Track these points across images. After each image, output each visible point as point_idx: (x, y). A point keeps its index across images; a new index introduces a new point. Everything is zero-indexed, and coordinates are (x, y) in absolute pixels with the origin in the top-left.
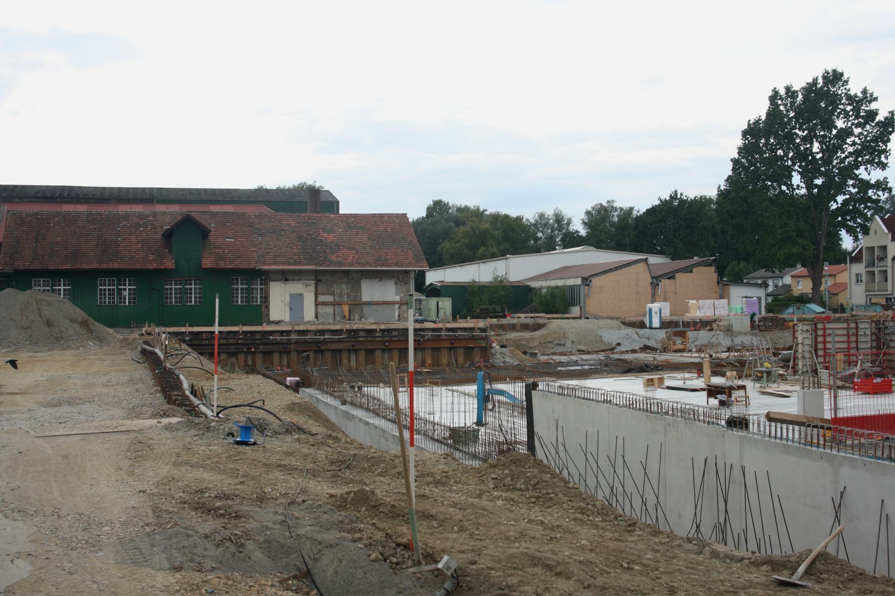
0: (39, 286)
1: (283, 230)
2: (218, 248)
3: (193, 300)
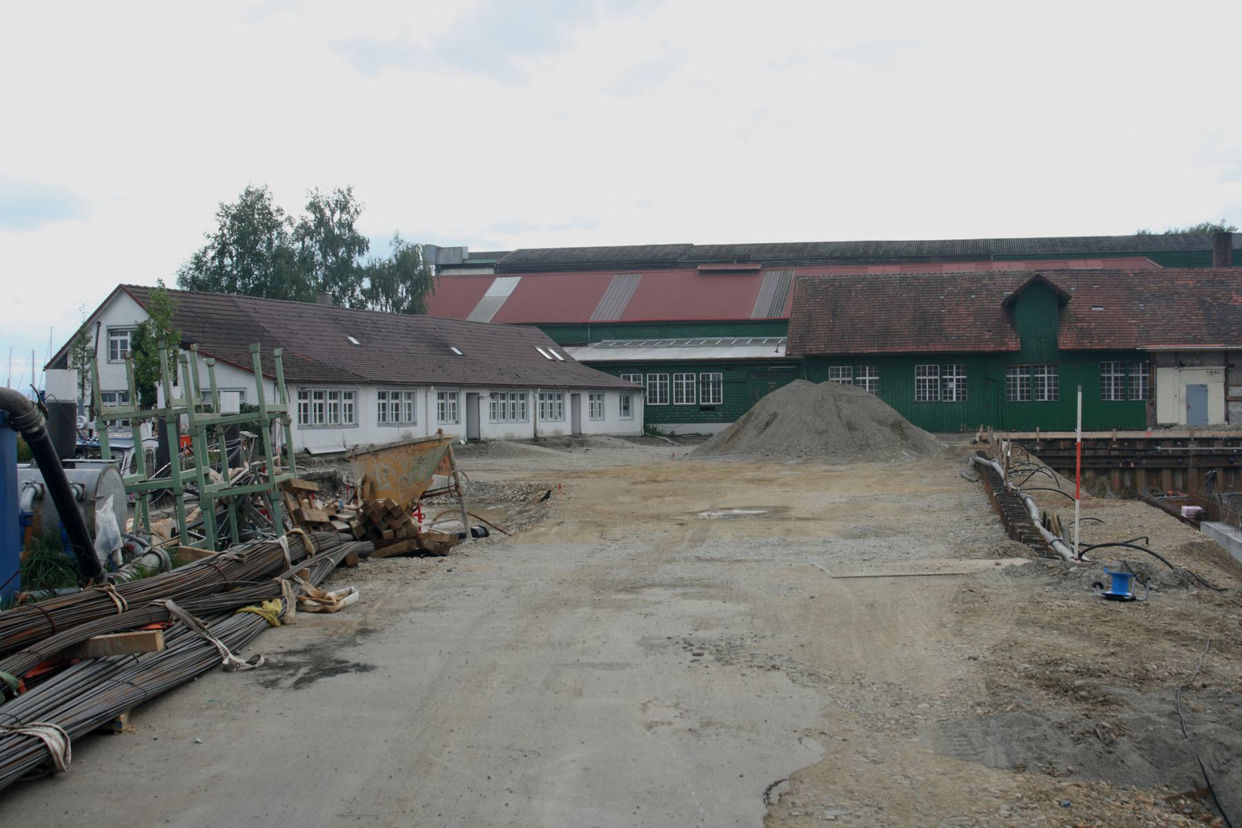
0: (838, 376)
1: (1176, 293)
3: (1046, 394)
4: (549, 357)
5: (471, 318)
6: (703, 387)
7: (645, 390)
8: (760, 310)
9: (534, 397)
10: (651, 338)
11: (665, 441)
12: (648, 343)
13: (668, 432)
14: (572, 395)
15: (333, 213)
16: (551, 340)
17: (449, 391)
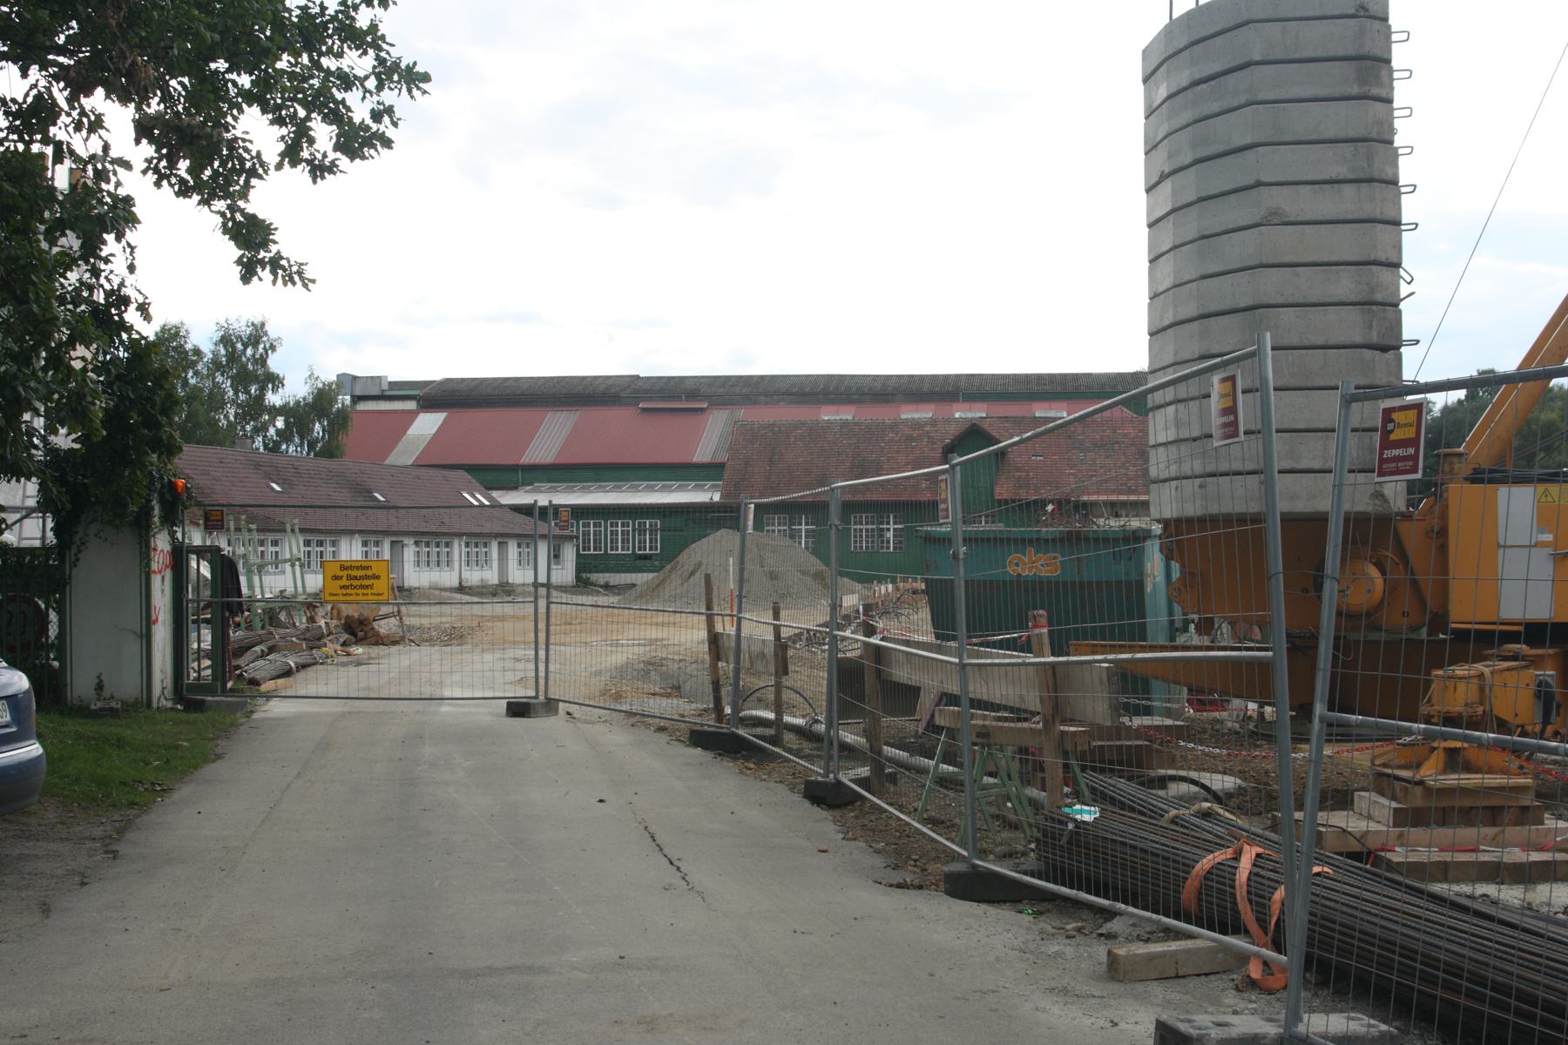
0: (773, 525)
1: (1117, 443)
2: (1018, 469)
4: (476, 503)
5: (388, 461)
6: (639, 535)
7: (577, 538)
8: (703, 452)
9: (460, 545)
10: (588, 481)
11: (598, 591)
12: (583, 488)
13: (602, 582)
14: (499, 543)
15: (245, 349)
16: (478, 484)
17: (373, 538)
